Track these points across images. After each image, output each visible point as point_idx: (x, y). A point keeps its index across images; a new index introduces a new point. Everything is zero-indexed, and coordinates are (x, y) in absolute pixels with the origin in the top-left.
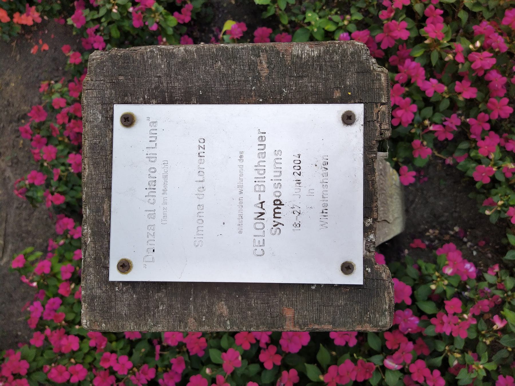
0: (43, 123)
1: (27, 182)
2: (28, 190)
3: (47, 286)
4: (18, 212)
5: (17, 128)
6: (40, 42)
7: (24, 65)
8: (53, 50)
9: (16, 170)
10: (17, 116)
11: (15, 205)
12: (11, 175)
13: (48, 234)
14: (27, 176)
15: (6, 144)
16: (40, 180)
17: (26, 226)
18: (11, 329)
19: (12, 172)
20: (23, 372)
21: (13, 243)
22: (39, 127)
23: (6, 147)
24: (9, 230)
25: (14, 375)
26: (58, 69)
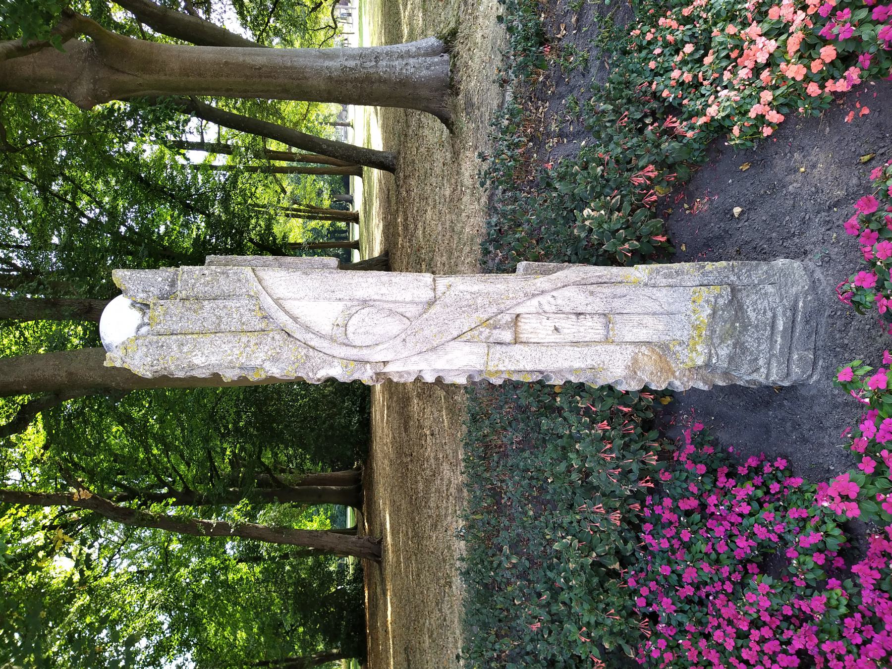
0: (873, 214)
1: (853, 285)
2: (854, 294)
3: (881, 405)
4: (830, 321)
5: (828, 219)
6: (858, 105)
7: (836, 138)
8: (877, 114)
9: (827, 271)
10: (828, 203)
11: (826, 314)
12: (822, 277)
13: (872, 349)
14: (852, 278)
15: (814, 239)
16: (870, 281)
17: (842, 338)
18: (821, 461)
19: (822, 273)
20: (853, 495)
21: (824, 359)
22: (867, 220)
23: (814, 243)
24: (820, 343)
25: (842, 497)
26: (884, 137)
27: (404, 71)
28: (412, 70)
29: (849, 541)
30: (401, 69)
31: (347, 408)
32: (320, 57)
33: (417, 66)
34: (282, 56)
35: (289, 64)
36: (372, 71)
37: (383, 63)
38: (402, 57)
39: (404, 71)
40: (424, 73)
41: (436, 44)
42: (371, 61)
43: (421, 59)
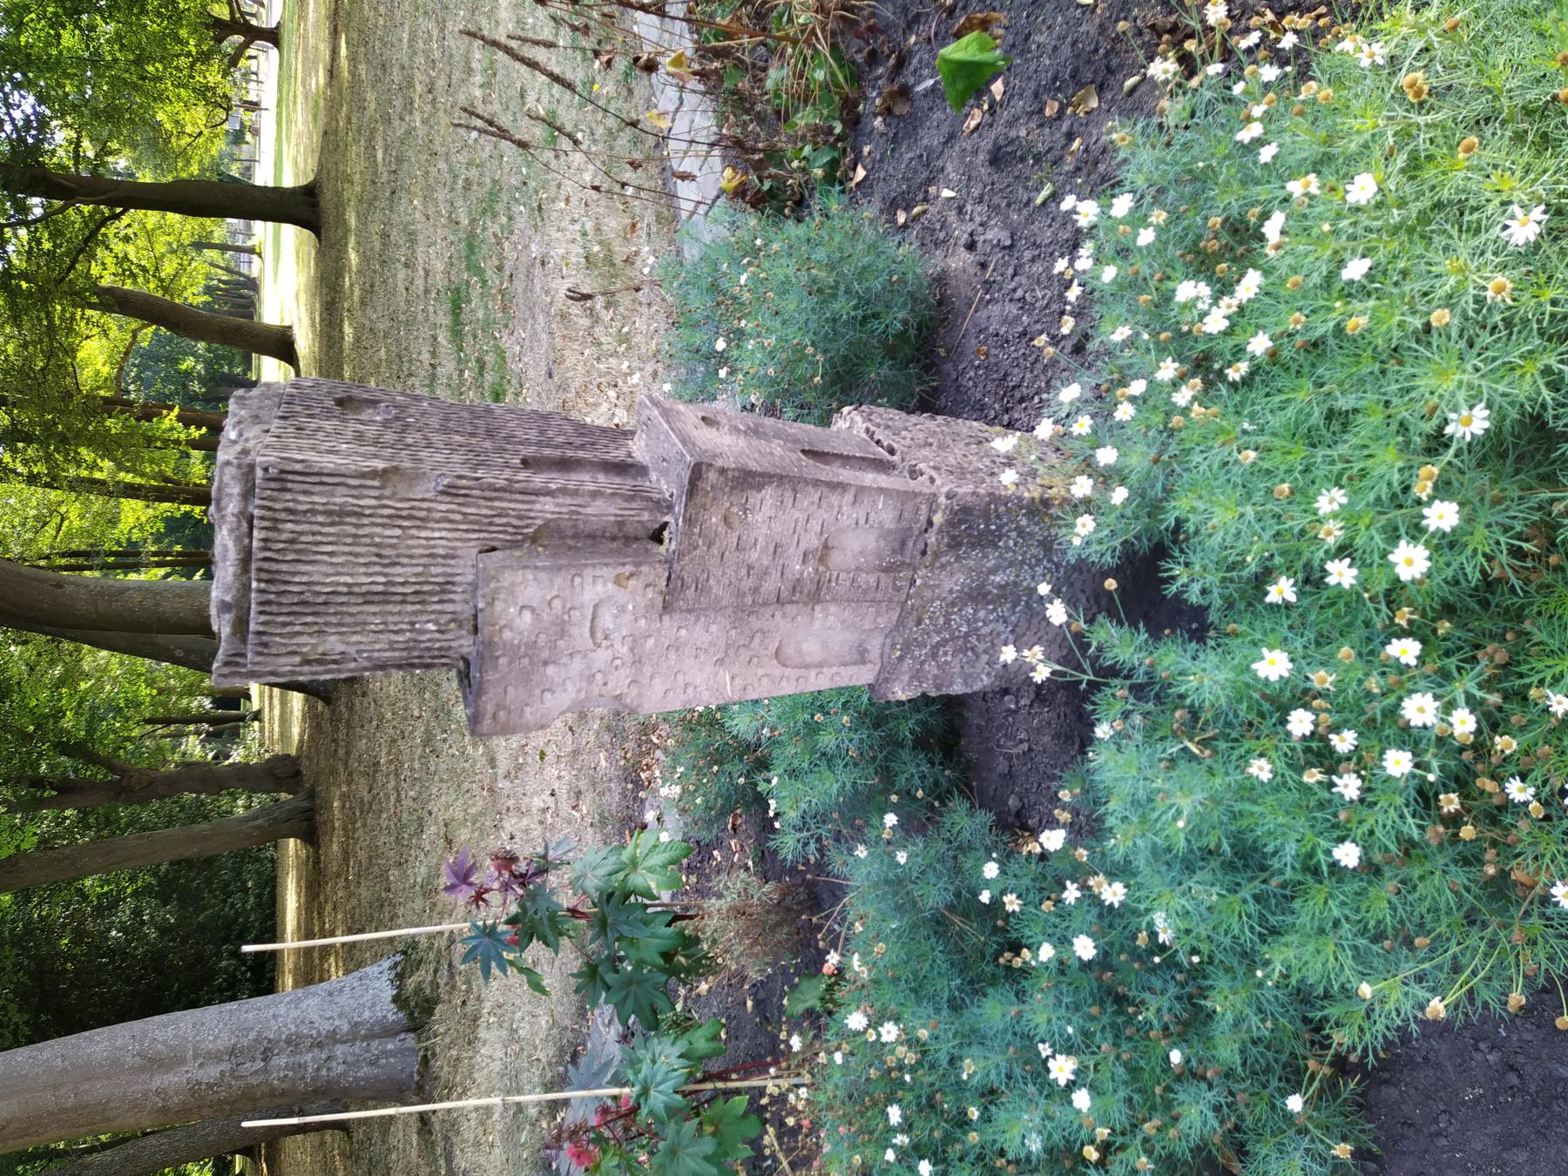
27: (324, 1072)
28: (341, 1069)
29: (720, 1144)
30: (318, 1069)
31: (226, 970)
32: (143, 1069)
33: (350, 1059)
34: (56, 1087)
35: (71, 1102)
36: (254, 1081)
37: (280, 1061)
38: (320, 1045)
39: (324, 1072)
40: (365, 1071)
41: (391, 1017)
42: (253, 1059)
43: (359, 1046)
